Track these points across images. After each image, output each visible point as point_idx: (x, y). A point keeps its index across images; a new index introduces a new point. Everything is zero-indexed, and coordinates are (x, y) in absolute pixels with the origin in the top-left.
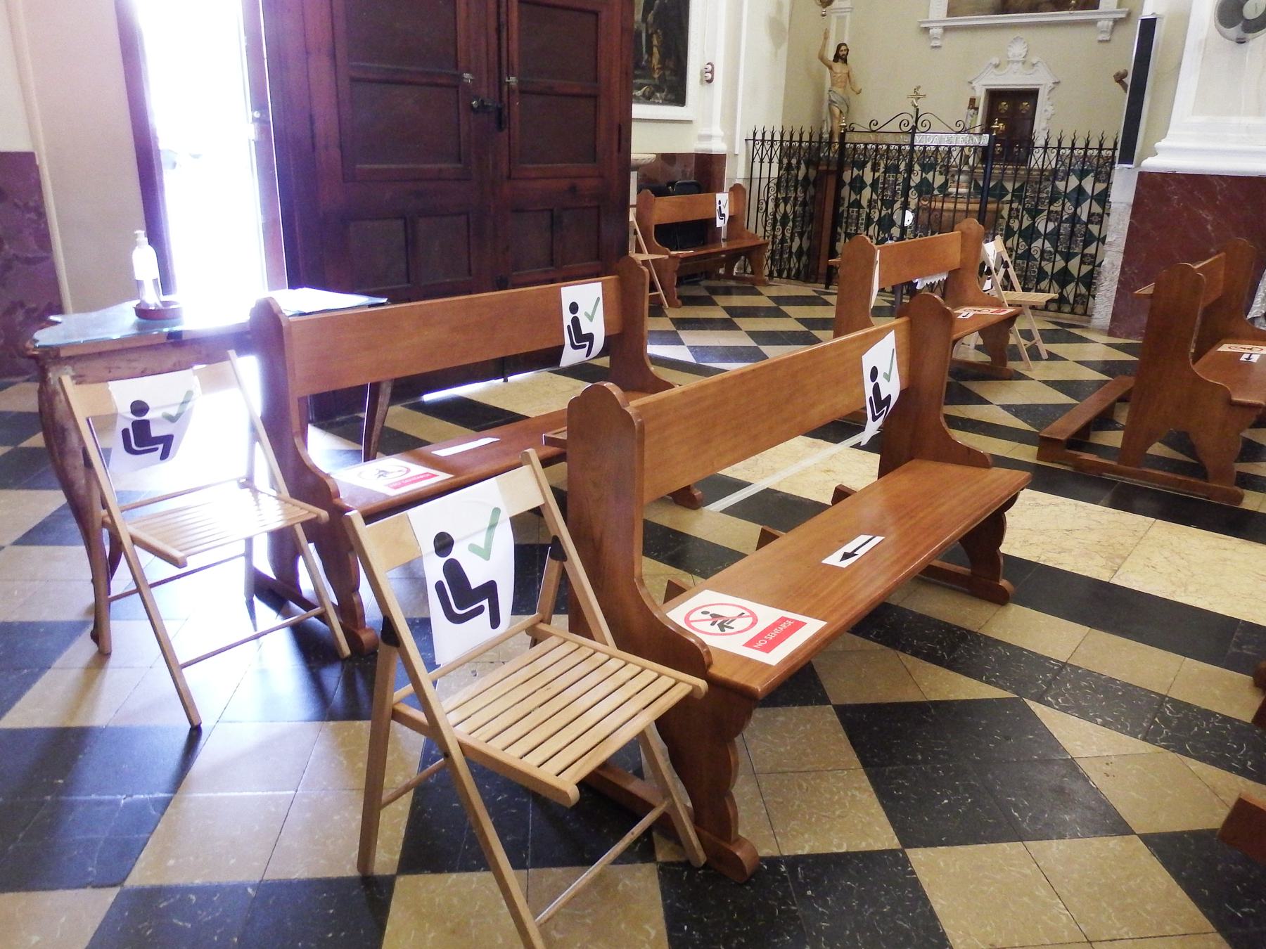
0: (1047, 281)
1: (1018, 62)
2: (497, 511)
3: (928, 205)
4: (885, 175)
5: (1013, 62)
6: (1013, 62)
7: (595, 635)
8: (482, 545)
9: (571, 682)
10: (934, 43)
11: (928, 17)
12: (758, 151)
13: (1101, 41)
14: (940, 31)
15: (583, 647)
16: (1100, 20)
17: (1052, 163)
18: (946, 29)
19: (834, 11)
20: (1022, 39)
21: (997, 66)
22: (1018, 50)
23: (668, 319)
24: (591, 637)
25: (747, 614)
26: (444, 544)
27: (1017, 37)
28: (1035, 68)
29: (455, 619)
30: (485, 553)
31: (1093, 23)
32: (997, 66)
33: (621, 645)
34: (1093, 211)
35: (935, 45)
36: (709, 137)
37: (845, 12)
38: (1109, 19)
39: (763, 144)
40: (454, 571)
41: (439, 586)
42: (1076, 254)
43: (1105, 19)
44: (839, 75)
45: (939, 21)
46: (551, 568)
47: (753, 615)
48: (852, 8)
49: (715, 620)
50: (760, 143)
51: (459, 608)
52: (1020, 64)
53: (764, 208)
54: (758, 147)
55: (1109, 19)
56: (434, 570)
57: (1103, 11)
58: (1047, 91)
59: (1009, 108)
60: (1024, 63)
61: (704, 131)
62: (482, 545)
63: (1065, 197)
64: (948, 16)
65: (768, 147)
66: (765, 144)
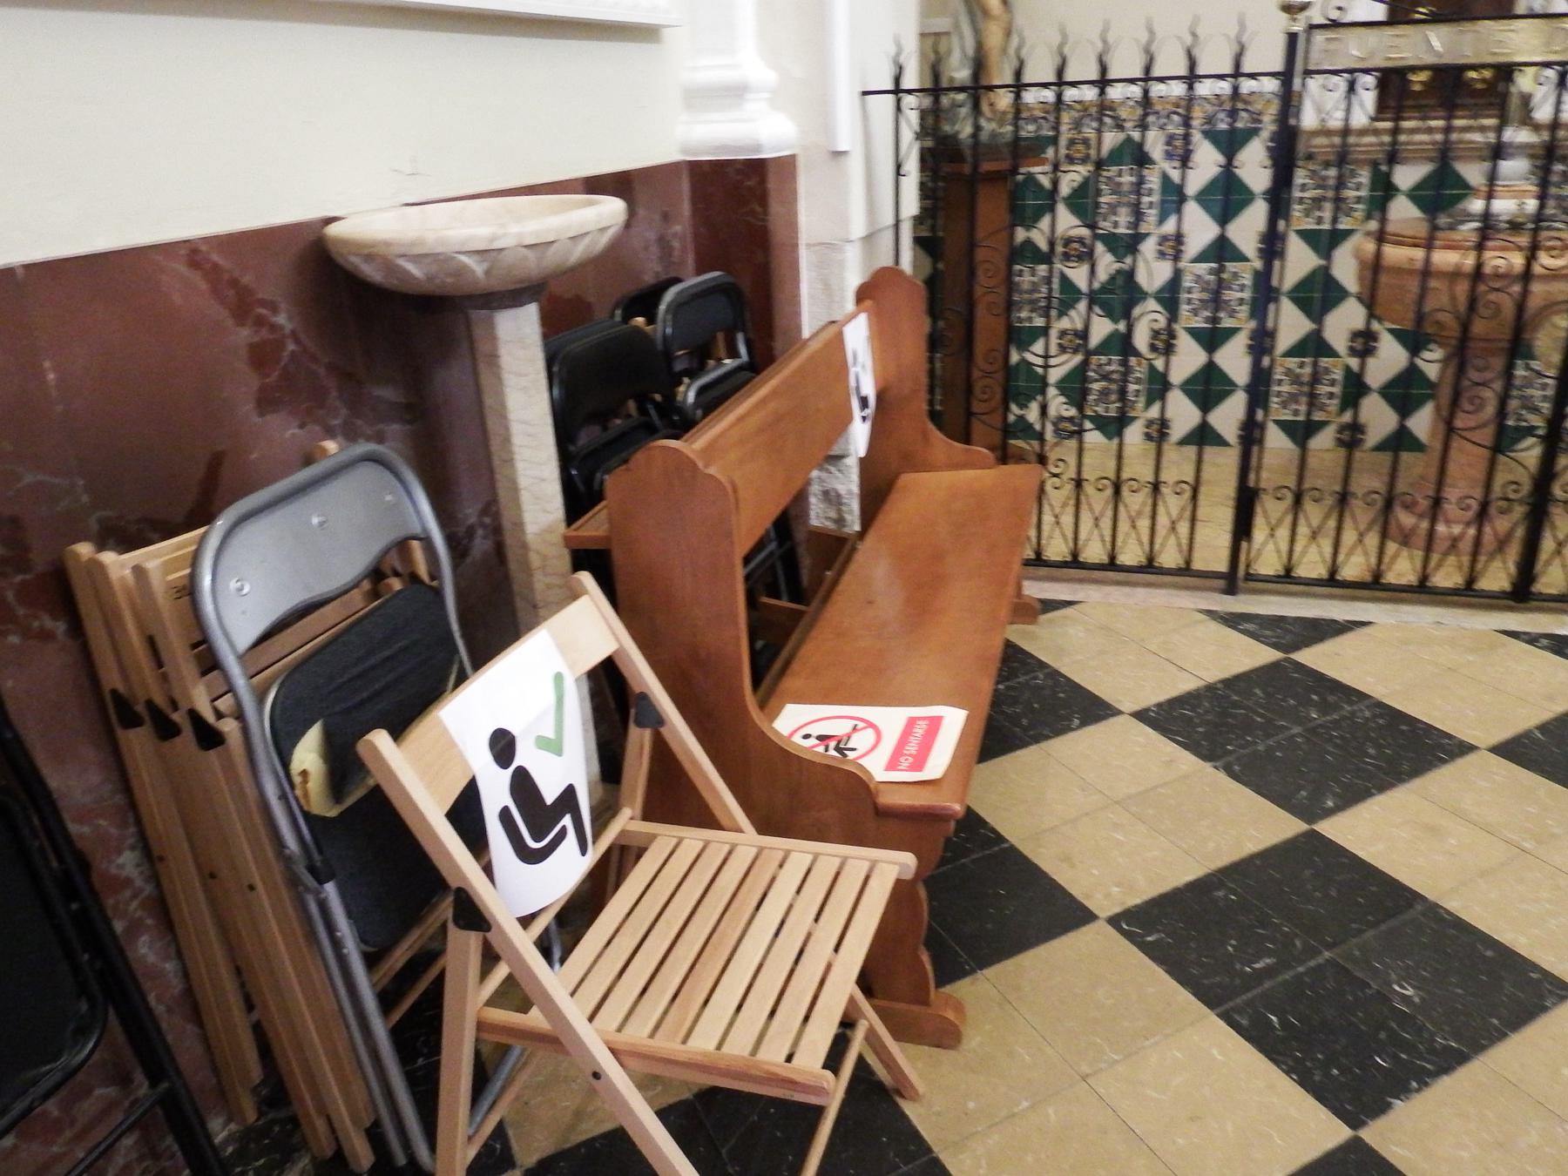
0: (1065, 189)
2: (559, 678)
7: (724, 821)
8: (551, 734)
9: (706, 900)
15: (821, 857)
23: (1484, 731)
24: (719, 827)
25: (861, 725)
26: (503, 746)
29: (530, 857)
30: (554, 746)
33: (765, 826)
36: (735, 93)
40: (523, 785)
41: (505, 815)
42: (1200, 258)
46: (639, 740)
47: (871, 725)
49: (825, 742)
51: (537, 840)
56: (496, 794)
61: (710, 71)
62: (551, 734)
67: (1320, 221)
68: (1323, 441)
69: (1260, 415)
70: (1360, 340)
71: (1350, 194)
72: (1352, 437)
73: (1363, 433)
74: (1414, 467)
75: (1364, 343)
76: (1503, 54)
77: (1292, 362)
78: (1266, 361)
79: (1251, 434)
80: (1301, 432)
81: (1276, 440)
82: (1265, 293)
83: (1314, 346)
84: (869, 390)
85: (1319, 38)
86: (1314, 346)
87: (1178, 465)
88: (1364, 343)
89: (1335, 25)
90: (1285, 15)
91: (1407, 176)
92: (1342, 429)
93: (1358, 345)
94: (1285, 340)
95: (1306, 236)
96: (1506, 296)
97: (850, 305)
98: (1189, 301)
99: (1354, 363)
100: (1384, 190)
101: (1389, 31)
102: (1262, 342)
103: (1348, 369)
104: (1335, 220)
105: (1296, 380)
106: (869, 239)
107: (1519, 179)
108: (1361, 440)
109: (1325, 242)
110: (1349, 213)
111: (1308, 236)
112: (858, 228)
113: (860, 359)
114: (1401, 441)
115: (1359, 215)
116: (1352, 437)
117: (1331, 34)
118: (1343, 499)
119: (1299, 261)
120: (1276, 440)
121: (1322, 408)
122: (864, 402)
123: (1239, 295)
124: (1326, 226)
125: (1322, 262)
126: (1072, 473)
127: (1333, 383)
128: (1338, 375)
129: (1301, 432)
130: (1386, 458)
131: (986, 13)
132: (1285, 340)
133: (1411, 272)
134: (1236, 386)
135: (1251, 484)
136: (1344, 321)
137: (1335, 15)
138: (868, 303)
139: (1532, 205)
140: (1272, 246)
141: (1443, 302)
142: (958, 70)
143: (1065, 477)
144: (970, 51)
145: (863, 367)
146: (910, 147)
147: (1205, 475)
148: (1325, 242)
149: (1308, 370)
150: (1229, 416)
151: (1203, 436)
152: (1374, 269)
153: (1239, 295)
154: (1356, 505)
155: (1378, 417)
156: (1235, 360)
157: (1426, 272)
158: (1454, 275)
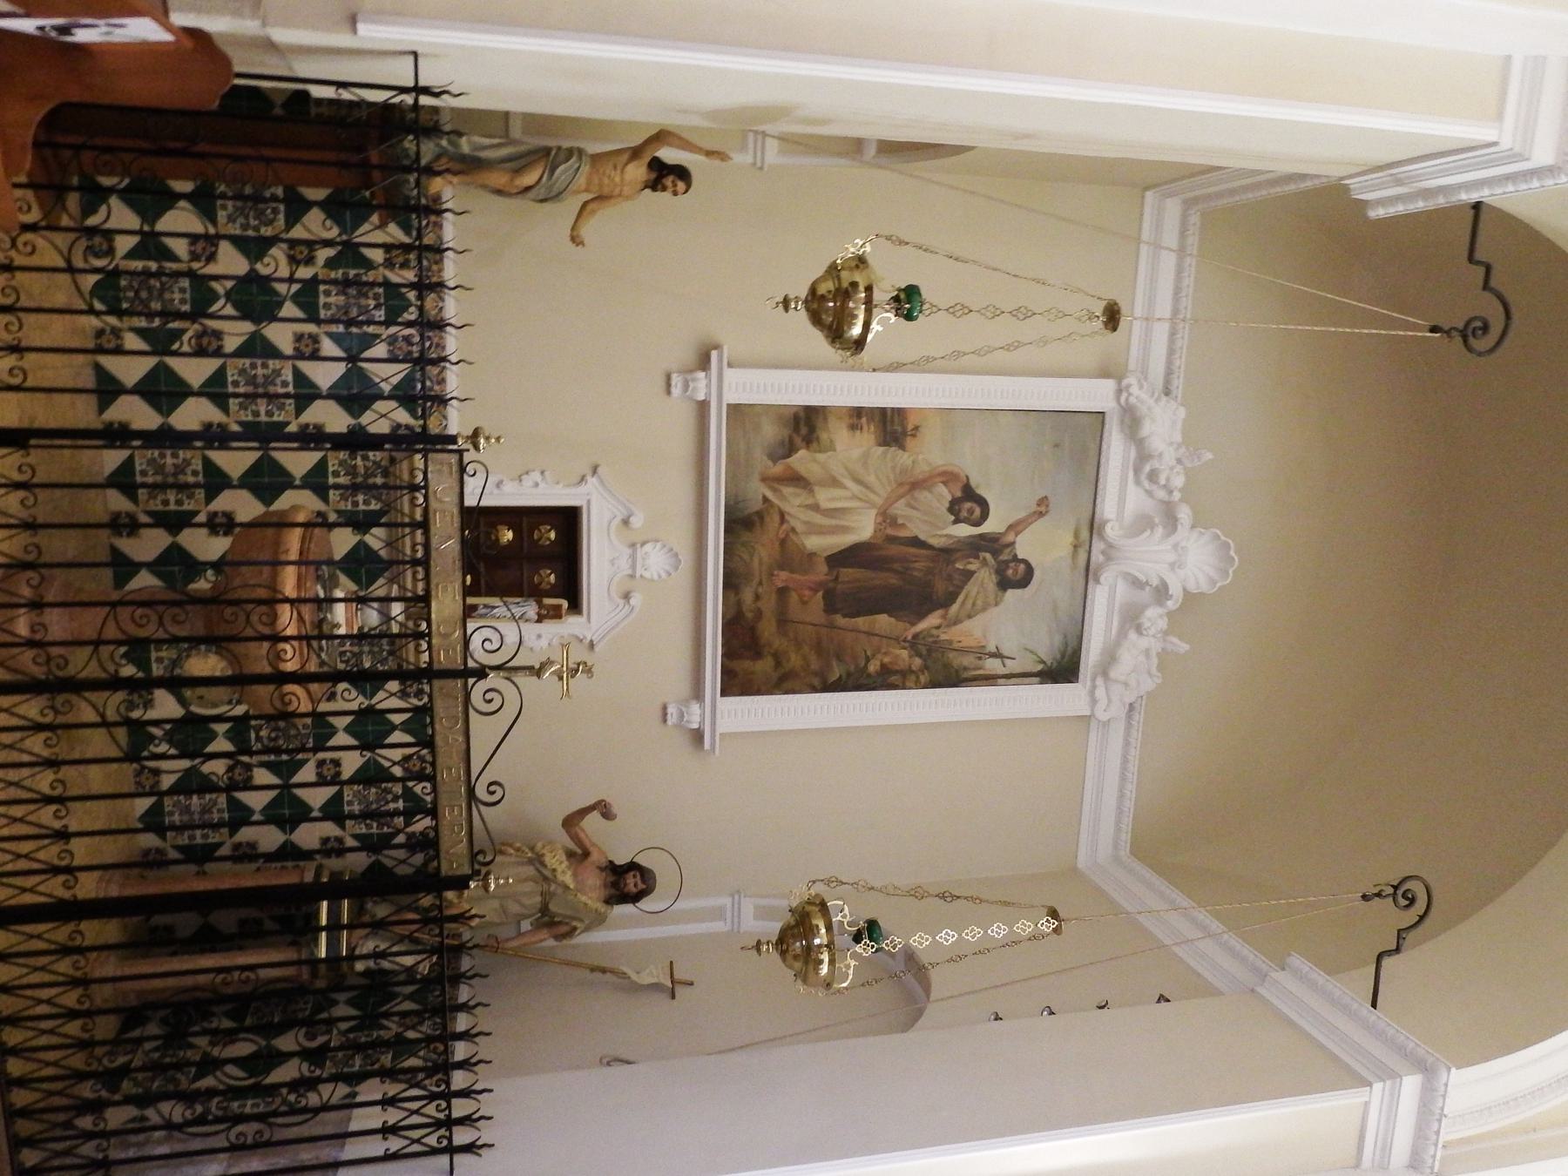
1: (633, 567)
3: (295, 643)
4: (380, 285)
5: (633, 557)
6: (633, 557)
10: (676, 380)
11: (730, 365)
12: (417, 1112)
13: (665, 708)
14: (701, 397)
16: (703, 708)
17: (414, 1116)
18: (703, 407)
19: (759, 144)
20: (676, 568)
21: (626, 522)
22: (655, 561)
27: (680, 561)
28: (621, 602)
31: (697, 693)
32: (626, 522)
34: (312, 778)
35: (673, 383)
37: (755, 153)
38: (708, 394)
39: (438, 1124)
43: (703, 715)
44: (617, 179)
45: (713, 723)
48: (761, 168)
50: (441, 1116)
52: (630, 572)
53: (255, 1126)
54: (431, 1110)
55: (708, 394)
57: (718, 704)
58: (578, 632)
59: (543, 546)
60: (632, 576)
63: (346, 244)
64: (728, 405)
65: (432, 1141)
66: (442, 1132)
67: (336, 474)
68: (117, 501)
69: (136, 443)
70: (223, 520)
71: (360, 498)
72: (125, 525)
73: (129, 535)
74: (100, 583)
75: (222, 524)
76: (437, 593)
77: (197, 465)
78: (198, 444)
79: (117, 435)
80: (123, 480)
81: (112, 459)
82: (264, 434)
83: (216, 481)
84: (82, 36)
85: (454, 459)
86: (216, 481)
87: (75, 371)
88: (222, 524)
89: (462, 469)
90: (470, 433)
91: (376, 539)
92: (131, 516)
93: (219, 520)
94: (219, 458)
95: (322, 465)
96: (243, 625)
97: (179, 19)
98: (254, 366)
99: (201, 518)
100: (361, 523)
101: (456, 511)
102: (215, 437)
103: (196, 513)
104: (337, 487)
105: (180, 469)
106: (270, 46)
107: (362, 621)
108: (121, 535)
109: (316, 481)
110: (344, 498)
111: (321, 467)
112: (281, 35)
113: (118, 31)
114: (124, 567)
115: (342, 506)
116: (125, 525)
117: (455, 468)
118: (30, 526)
119: (299, 462)
120: (112, 459)
121: (152, 497)
122: (65, 30)
123: (263, 412)
124: (139, 479)
125: (235, 483)
126: (19, 260)
127: (179, 502)
128: (188, 506)
129: (123, 480)
130: (104, 556)
131: (518, 172)
132: (219, 458)
133: (276, 552)
134: (169, 415)
135: (33, 442)
136: (244, 506)
137: (470, 469)
138: (188, 44)
139: (342, 631)
140: (312, 438)
141: (250, 582)
142: (469, 142)
143: (13, 253)
144: (484, 154)
145: (108, 33)
146: (355, 94)
147: (57, 397)
148: (316, 481)
149: (191, 479)
150: (139, 414)
151: (108, 389)
152: (282, 523)
153: (263, 412)
154: (24, 538)
155: (149, 544)
156: (192, 415)
157: (277, 564)
158: (273, 586)
